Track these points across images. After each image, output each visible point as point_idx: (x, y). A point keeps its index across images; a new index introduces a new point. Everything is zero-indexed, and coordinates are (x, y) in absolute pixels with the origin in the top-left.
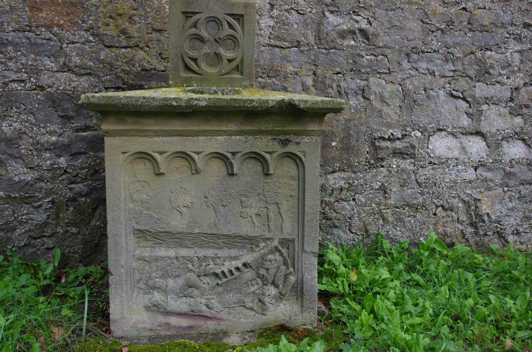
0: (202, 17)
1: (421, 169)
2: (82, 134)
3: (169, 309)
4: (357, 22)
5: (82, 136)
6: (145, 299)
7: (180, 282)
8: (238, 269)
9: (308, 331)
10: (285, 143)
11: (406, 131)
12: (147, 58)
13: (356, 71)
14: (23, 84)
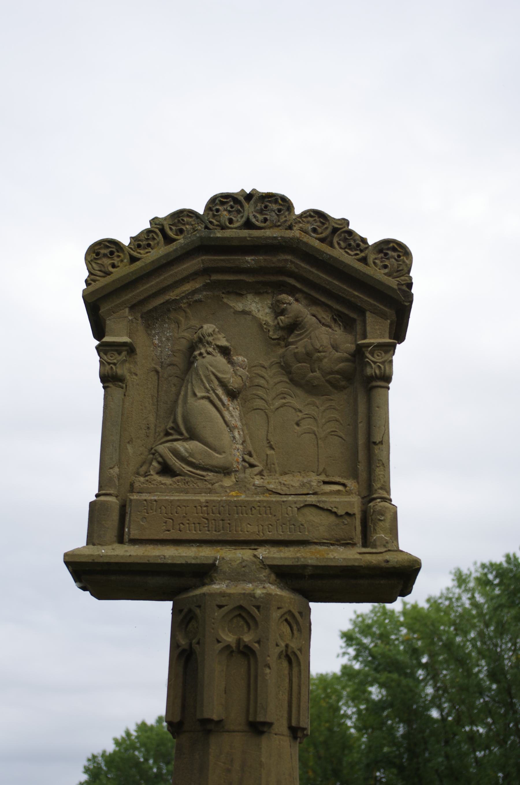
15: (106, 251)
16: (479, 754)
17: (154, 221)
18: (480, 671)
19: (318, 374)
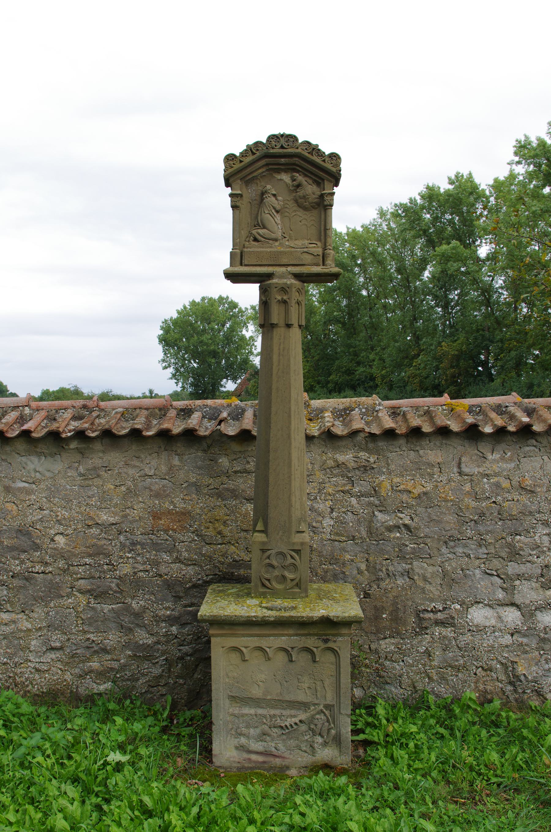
0: (273, 552)
1: (461, 636)
2: (189, 609)
3: (250, 749)
4: (401, 519)
5: (189, 610)
6: (235, 742)
7: (258, 731)
8: (296, 724)
9: (344, 769)
10: (326, 641)
11: (446, 604)
12: (237, 551)
13: (402, 557)
14: (147, 573)
15: (231, 158)
16: (389, 315)
17: (248, 146)
18: (391, 268)
19: (307, 203)
